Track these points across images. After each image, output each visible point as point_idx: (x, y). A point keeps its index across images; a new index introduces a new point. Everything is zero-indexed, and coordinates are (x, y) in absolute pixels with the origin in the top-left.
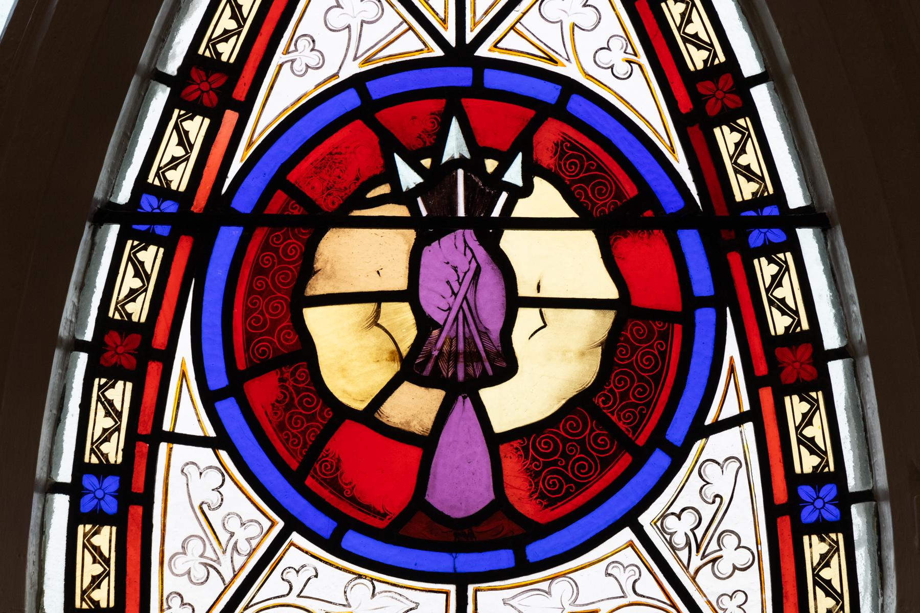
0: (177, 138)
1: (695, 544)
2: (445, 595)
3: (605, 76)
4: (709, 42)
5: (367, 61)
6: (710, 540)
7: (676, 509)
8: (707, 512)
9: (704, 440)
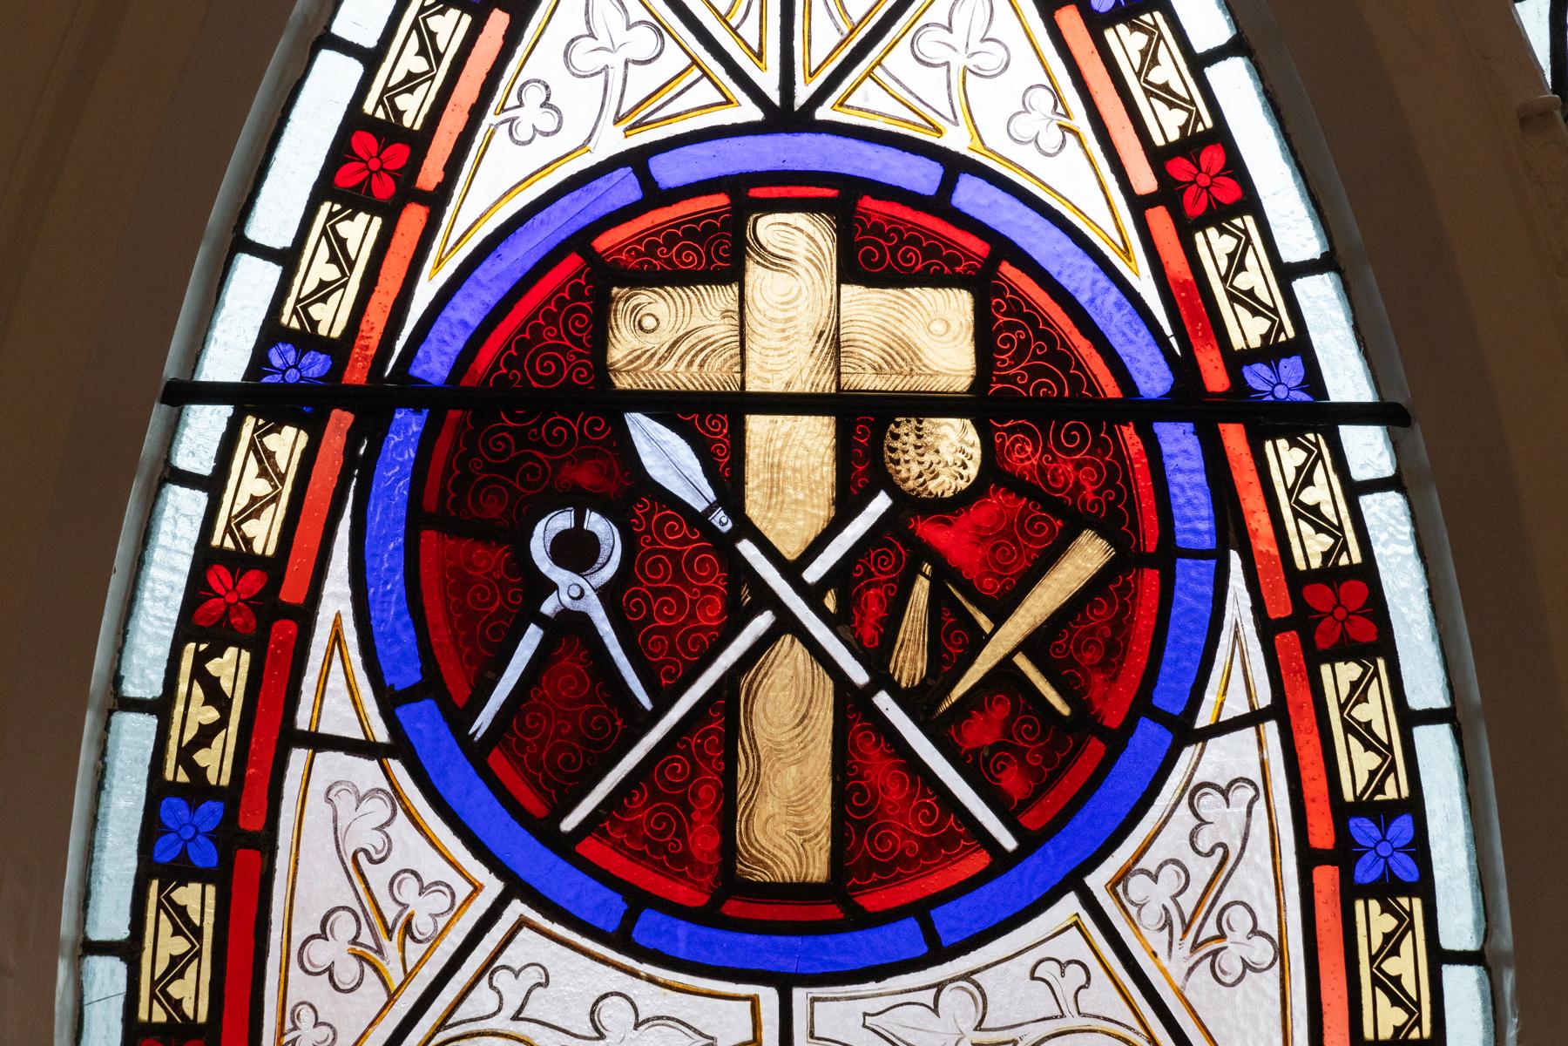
2: (471, 889)
4: (1415, 998)
6: (1205, 919)
7: (1149, 862)
8: (1202, 870)
9: (1200, 745)
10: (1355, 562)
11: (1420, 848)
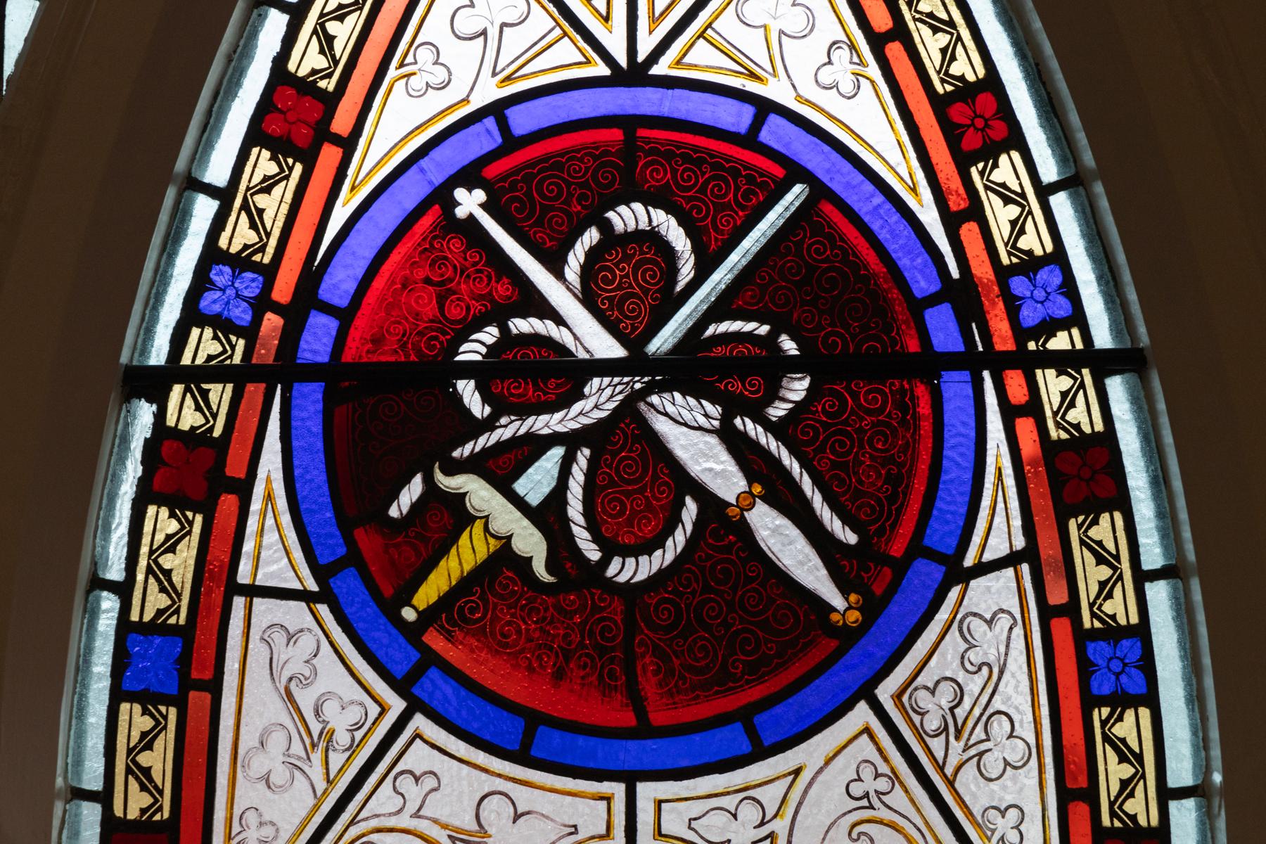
0: (247, 221)
1: (954, 728)
3: (829, 100)
5: (508, 79)
7: (925, 679)
10: (1096, 430)
11: (1070, 288)
